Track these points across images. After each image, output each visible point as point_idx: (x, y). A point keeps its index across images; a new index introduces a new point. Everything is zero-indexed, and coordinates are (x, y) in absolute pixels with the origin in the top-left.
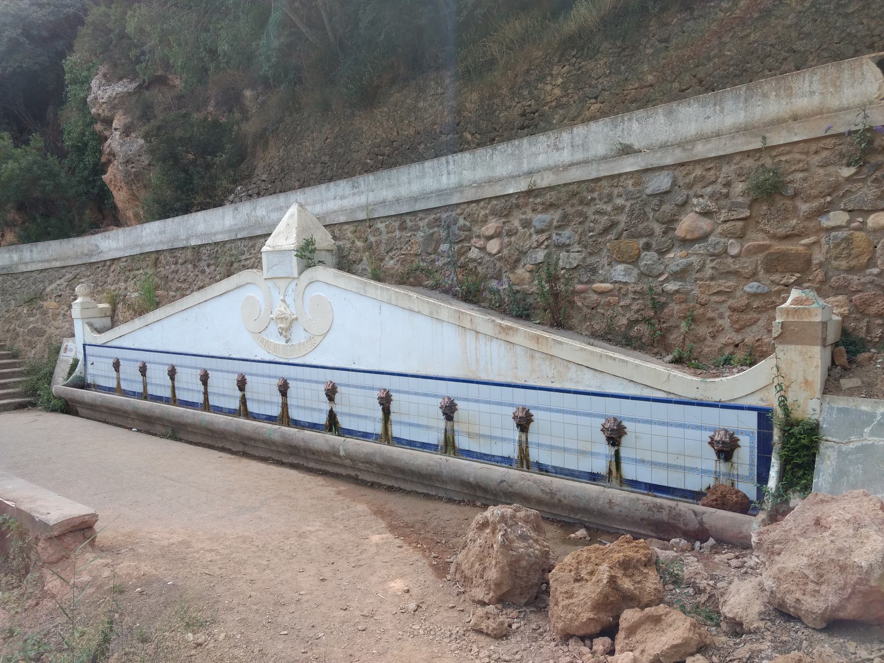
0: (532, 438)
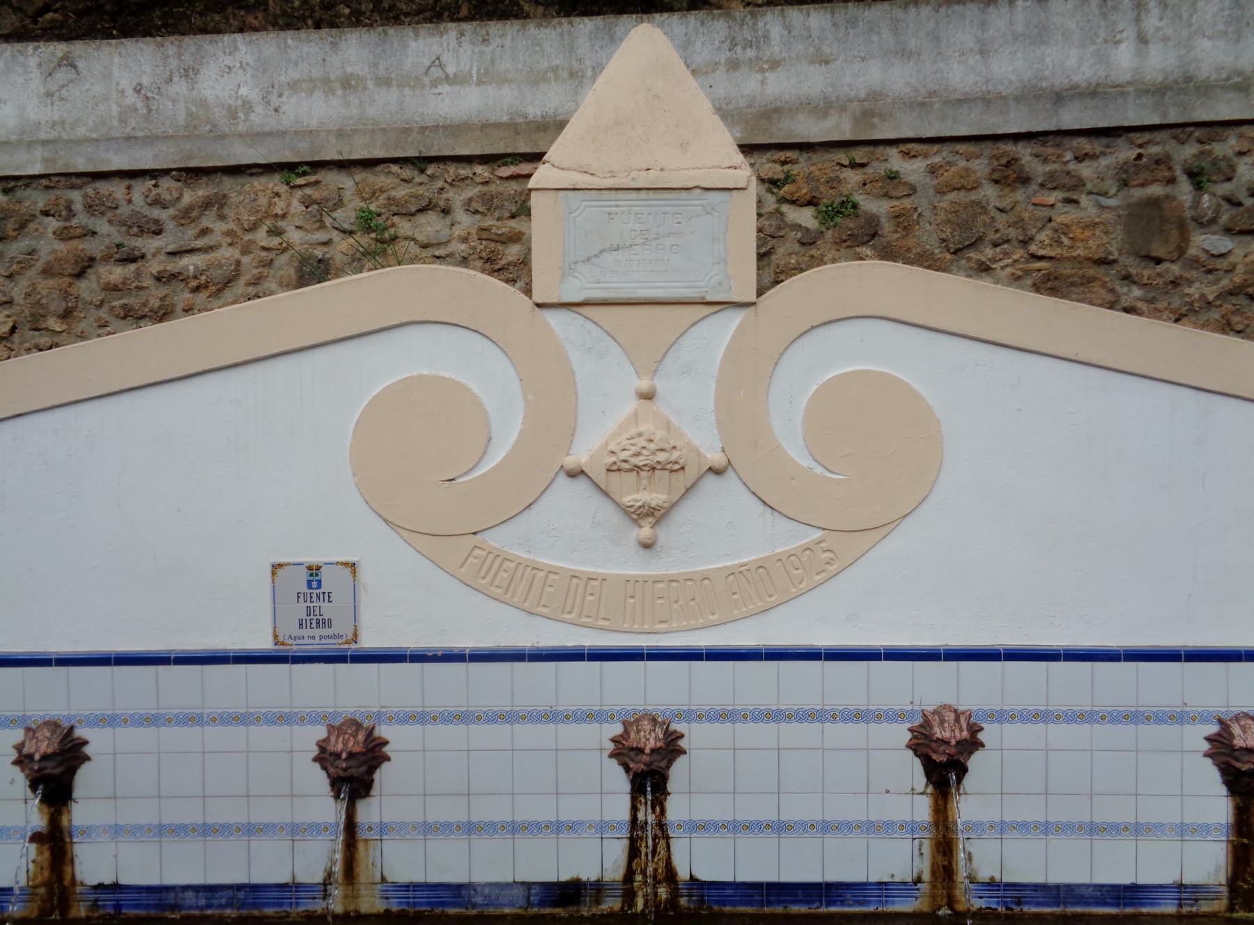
0: (676, 809)
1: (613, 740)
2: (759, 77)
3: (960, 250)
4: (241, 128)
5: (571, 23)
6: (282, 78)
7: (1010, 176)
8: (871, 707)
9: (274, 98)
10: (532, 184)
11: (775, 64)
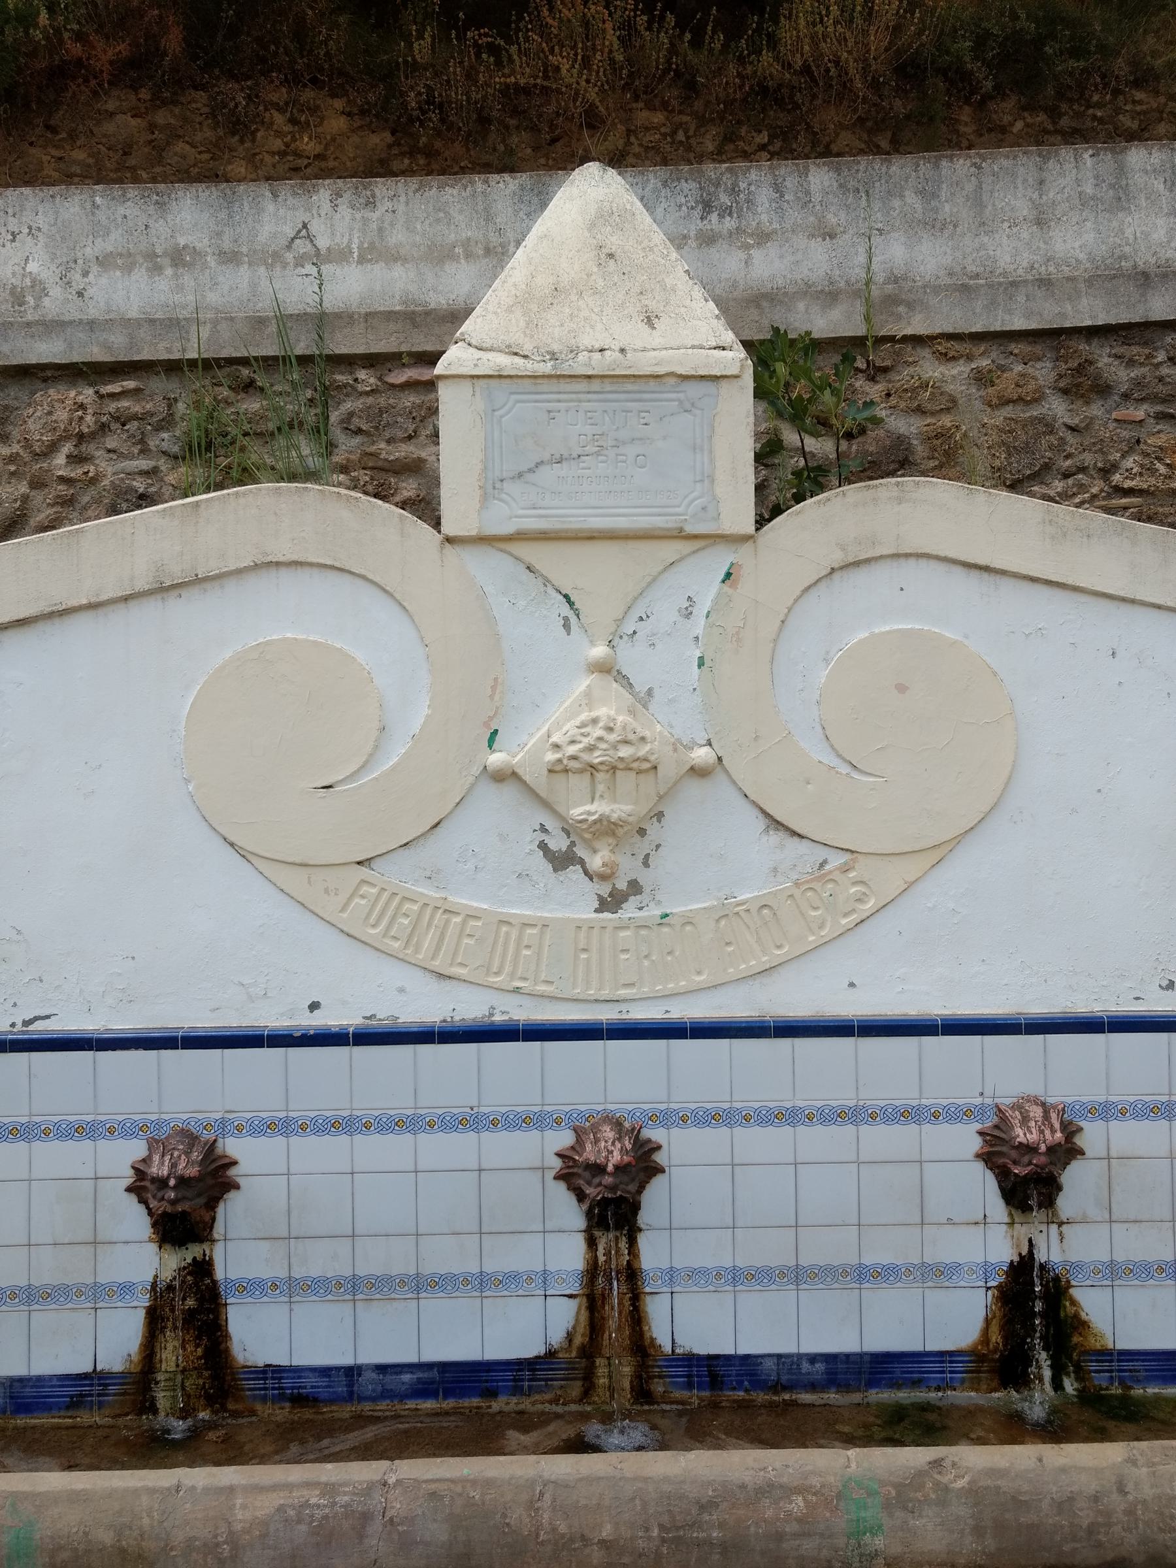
0: (653, 1253)
1: (559, 1155)
2: (742, 255)
3: (1020, 481)
4: (30, 317)
5: (486, 181)
6: (88, 250)
7: (1083, 385)
8: (924, 1102)
9: (76, 276)
10: (439, 369)
11: (763, 237)
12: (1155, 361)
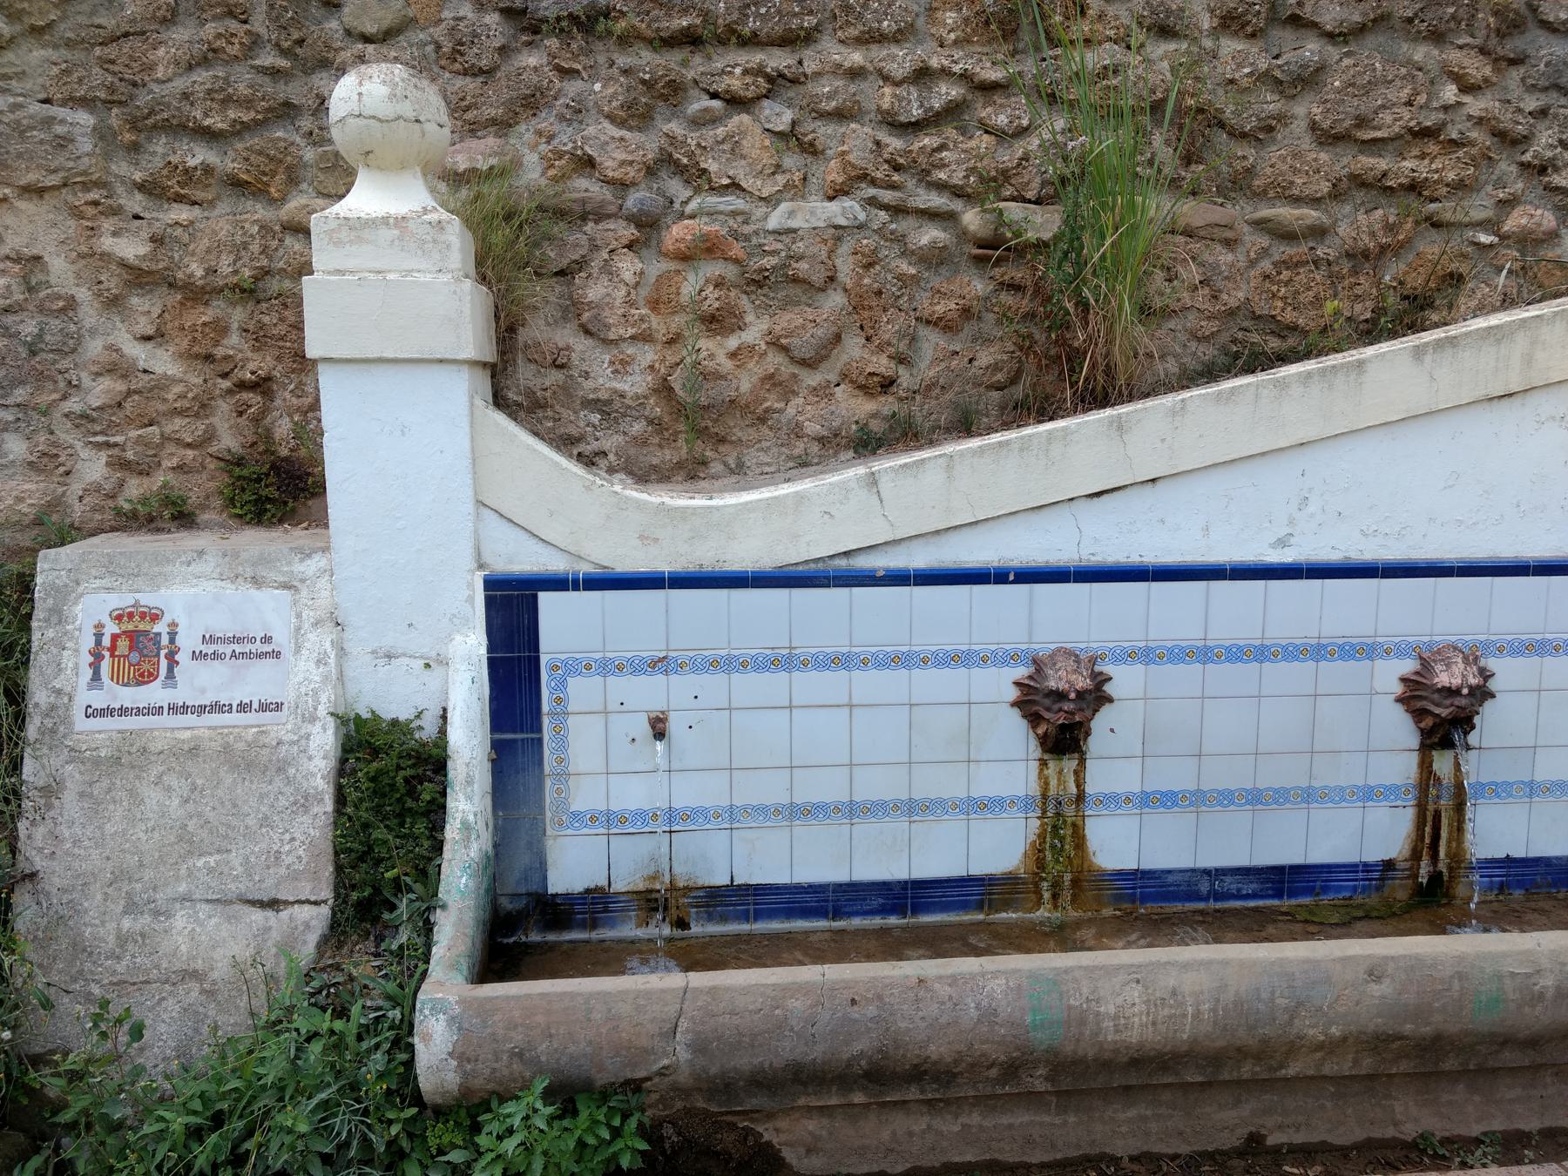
12: (714, 269)
